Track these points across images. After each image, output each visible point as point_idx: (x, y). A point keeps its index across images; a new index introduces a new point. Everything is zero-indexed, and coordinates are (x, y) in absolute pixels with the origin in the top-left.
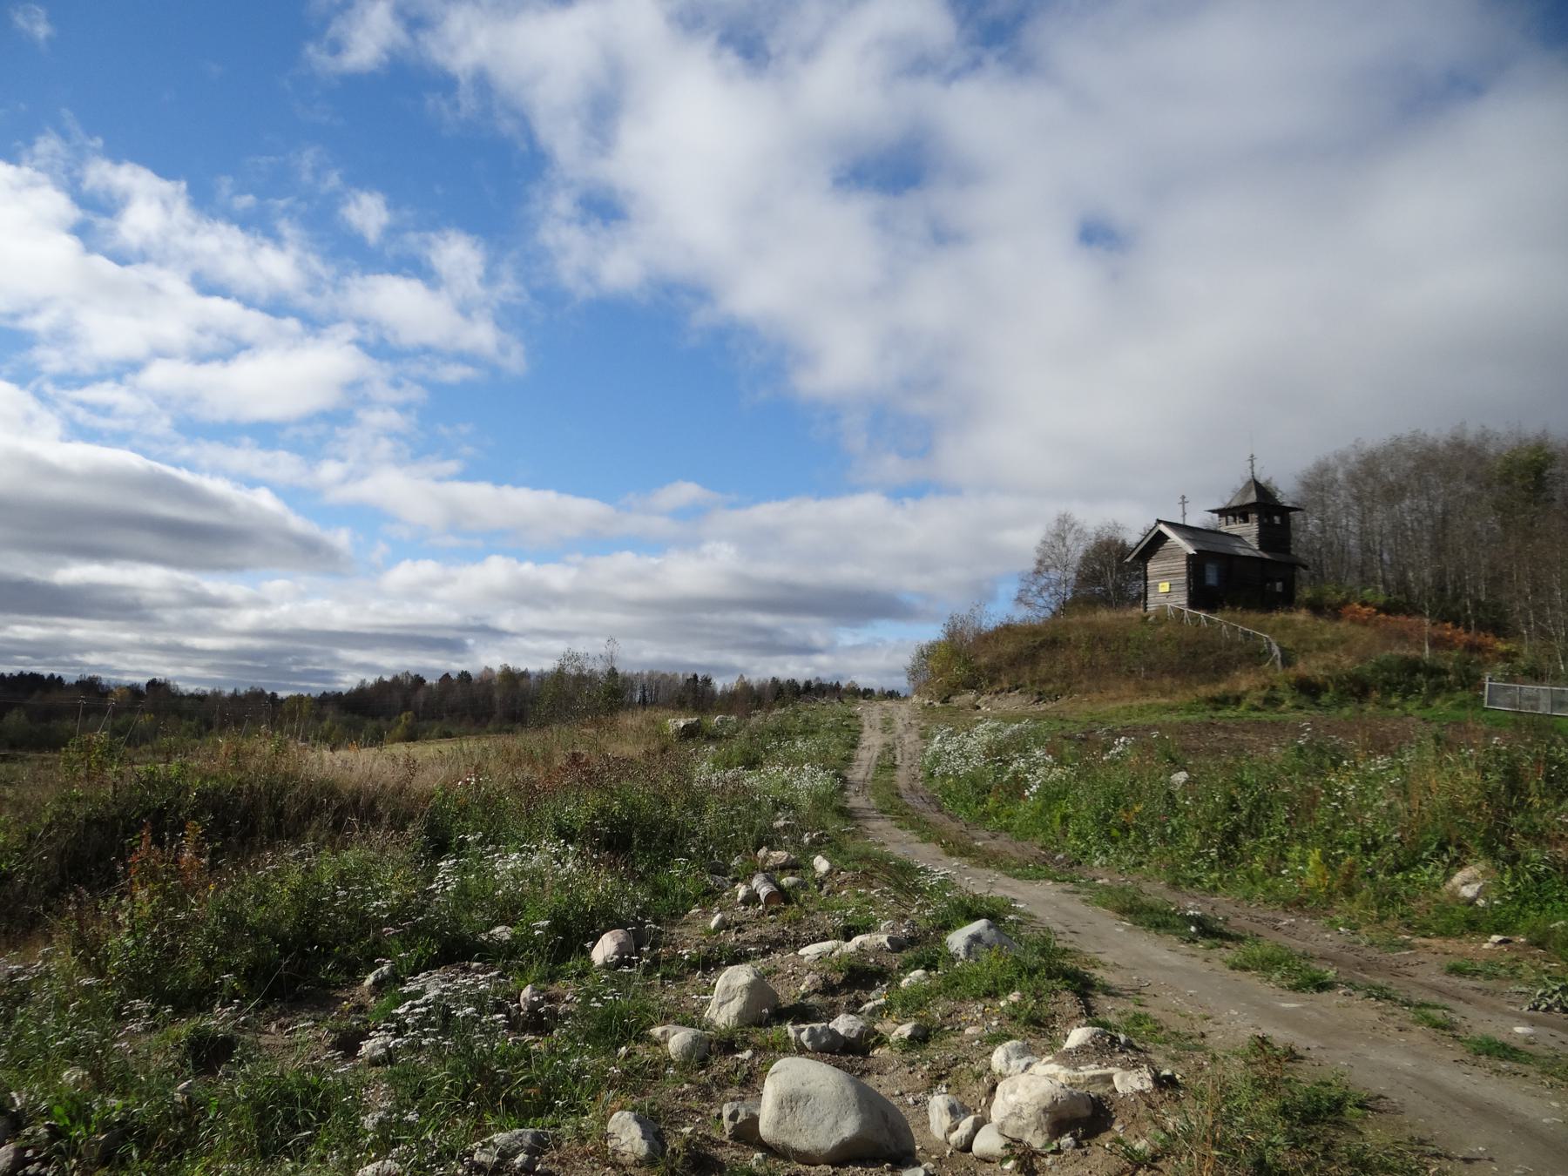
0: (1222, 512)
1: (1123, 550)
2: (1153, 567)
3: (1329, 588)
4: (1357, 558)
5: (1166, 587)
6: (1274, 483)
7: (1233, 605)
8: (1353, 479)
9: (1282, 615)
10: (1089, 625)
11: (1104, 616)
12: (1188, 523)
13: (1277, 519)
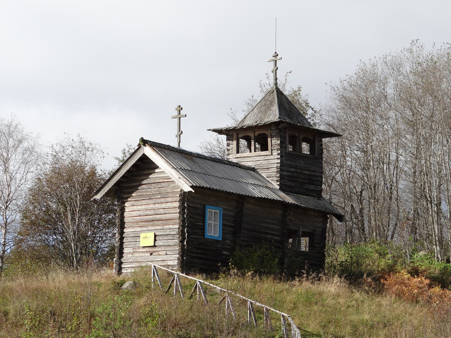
0: (231, 133)
1: (91, 182)
2: (133, 209)
3: (370, 249)
4: (407, 205)
5: (150, 237)
6: (303, 95)
7: (242, 267)
8: (407, 96)
9: (306, 284)
10: (37, 293)
11: (59, 279)
12: (185, 146)
13: (305, 148)
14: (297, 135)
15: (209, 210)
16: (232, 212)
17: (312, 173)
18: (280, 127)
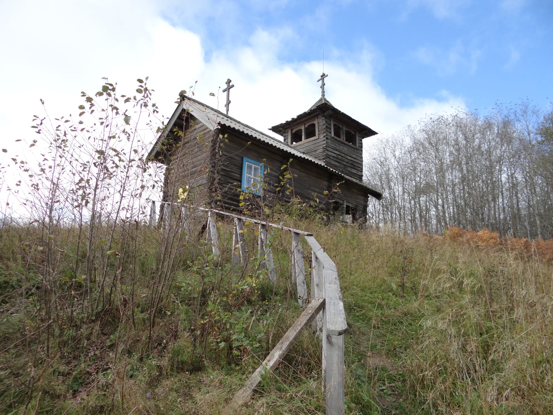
14: (341, 127)
15: (247, 163)
16: (276, 172)
17: (355, 160)
18: (325, 114)
